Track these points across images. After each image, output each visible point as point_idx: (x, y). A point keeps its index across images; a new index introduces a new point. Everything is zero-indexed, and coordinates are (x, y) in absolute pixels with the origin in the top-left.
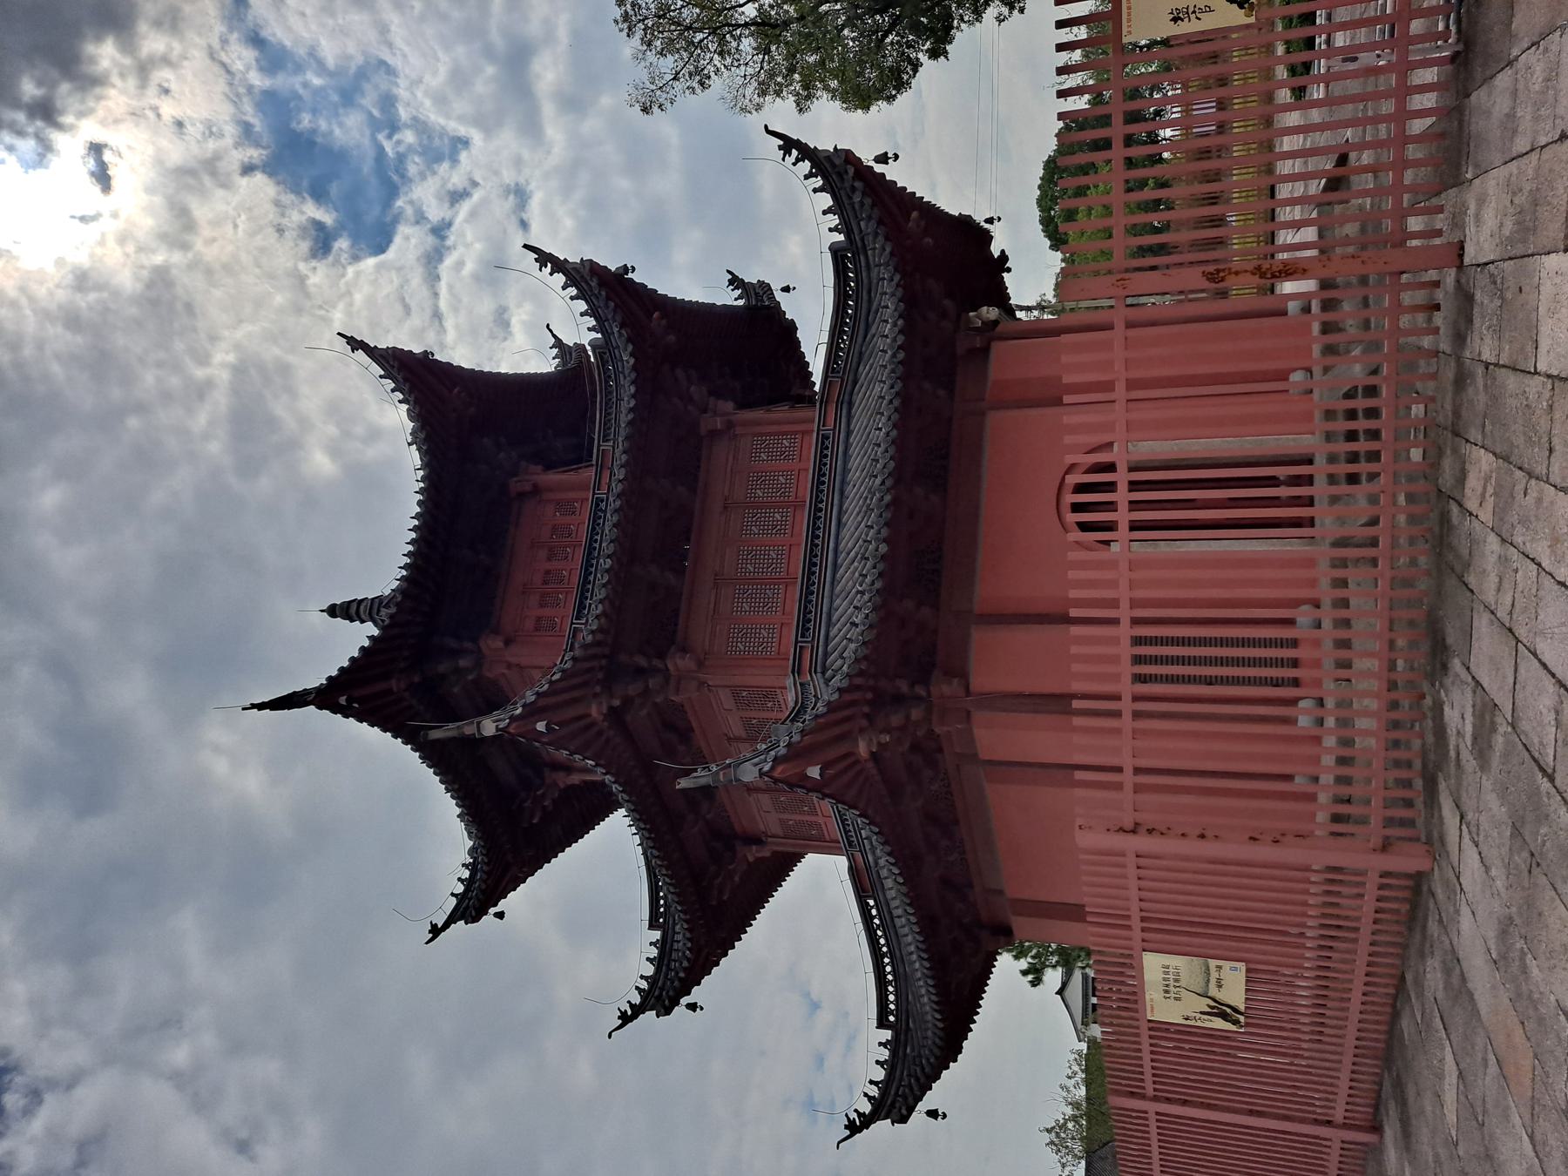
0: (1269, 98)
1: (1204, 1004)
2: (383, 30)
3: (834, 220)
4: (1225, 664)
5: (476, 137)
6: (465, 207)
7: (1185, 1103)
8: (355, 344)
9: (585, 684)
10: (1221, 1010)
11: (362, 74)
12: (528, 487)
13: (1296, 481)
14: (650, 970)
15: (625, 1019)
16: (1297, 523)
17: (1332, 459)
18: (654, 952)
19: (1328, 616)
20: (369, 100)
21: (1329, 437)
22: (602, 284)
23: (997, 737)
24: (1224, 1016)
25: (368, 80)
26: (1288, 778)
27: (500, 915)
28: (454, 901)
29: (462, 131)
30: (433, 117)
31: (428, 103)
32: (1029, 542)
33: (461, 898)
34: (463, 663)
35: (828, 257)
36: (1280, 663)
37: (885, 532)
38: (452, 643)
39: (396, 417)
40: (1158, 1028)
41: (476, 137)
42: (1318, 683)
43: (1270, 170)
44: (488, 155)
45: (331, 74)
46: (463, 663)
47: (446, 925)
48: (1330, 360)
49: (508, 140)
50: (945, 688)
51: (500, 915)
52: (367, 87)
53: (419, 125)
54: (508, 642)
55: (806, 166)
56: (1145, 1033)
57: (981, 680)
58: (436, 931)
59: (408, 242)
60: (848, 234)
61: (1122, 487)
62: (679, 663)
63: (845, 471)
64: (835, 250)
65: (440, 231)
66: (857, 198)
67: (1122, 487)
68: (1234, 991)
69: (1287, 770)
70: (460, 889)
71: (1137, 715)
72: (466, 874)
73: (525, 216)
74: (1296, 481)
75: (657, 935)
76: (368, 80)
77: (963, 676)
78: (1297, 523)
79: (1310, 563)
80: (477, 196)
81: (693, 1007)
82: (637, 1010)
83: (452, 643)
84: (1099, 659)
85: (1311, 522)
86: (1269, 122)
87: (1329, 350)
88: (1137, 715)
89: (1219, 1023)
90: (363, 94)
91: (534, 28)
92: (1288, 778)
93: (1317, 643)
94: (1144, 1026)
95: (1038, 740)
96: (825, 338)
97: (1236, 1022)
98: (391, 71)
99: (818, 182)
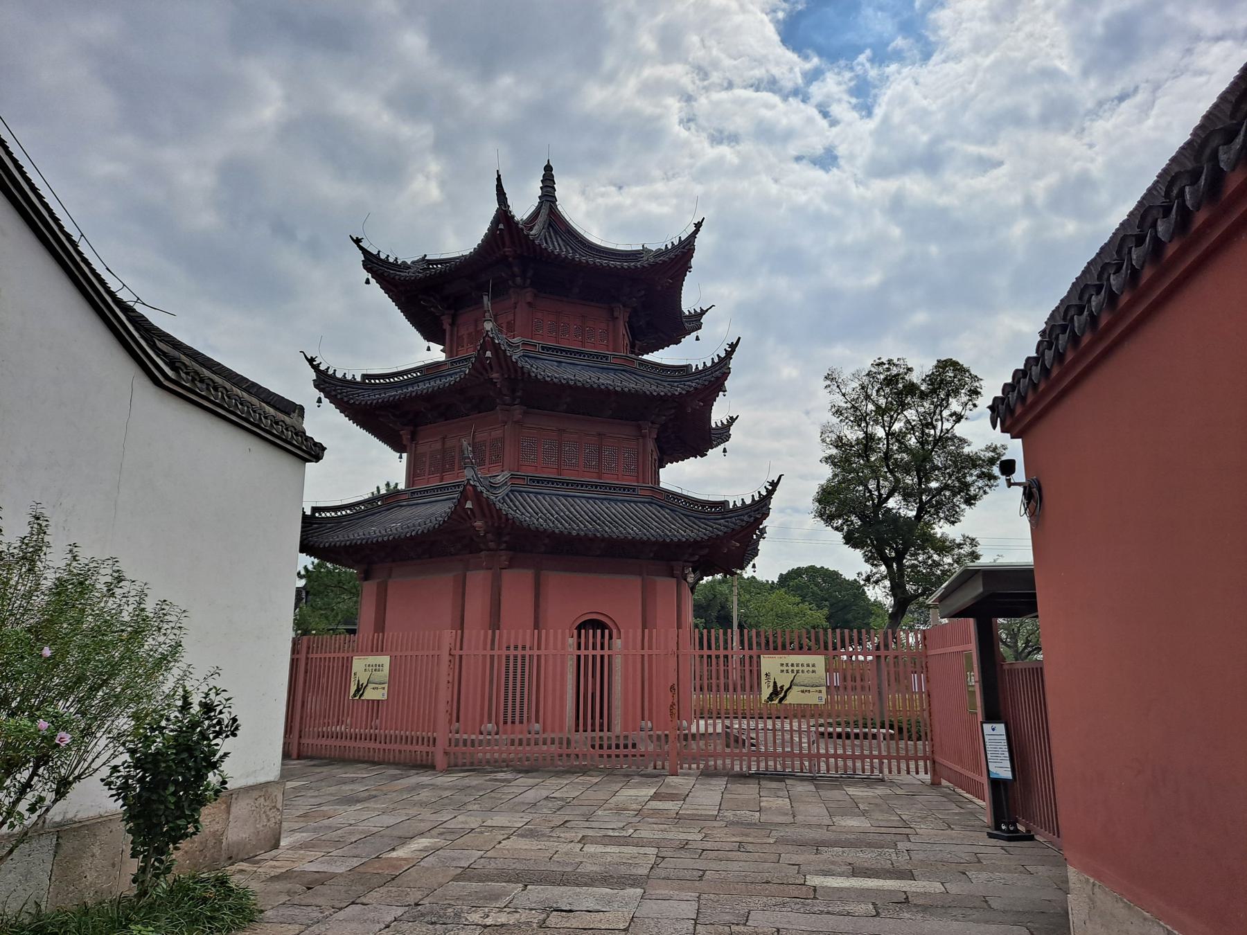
0: (812, 716)
1: (364, 681)
2: (957, 57)
3: (739, 504)
4: (515, 695)
5: (872, 124)
6: (814, 113)
7: (306, 672)
8: (698, 226)
9: (509, 369)
10: (360, 689)
11: (920, 38)
12: (616, 314)
13: (601, 725)
14: (339, 375)
15: (311, 361)
16: (577, 725)
17: (609, 738)
18: (349, 377)
19: (541, 736)
20: (900, 42)
21: (618, 737)
22: (717, 378)
23: (478, 581)
24: (358, 690)
25: (917, 41)
26: (458, 721)
27: (368, 282)
28: (375, 253)
29: (879, 112)
30: (889, 92)
31: (899, 88)
32: (573, 594)
33: (377, 256)
34: (518, 280)
35: (722, 499)
36: (521, 716)
37: (582, 533)
38: (530, 274)
39: (659, 240)
40: (349, 661)
41: (872, 124)
42: (505, 733)
43: (795, 716)
44: (856, 134)
45: (923, 15)
46: (518, 280)
47: (361, 248)
48: (655, 738)
49: (865, 151)
50: (504, 557)
51: (368, 282)
52: (911, 41)
53: (884, 79)
54: (529, 304)
55: (764, 493)
56: (345, 655)
57: (508, 576)
58: (357, 241)
59: (789, 65)
60: (731, 511)
61: (602, 652)
62: (517, 411)
63: (616, 501)
64: (725, 503)
65: (800, 93)
66: (746, 518)
67: (602, 652)
68: (370, 694)
69: (541, 720)
70: (383, 256)
71: (508, 657)
72: (391, 260)
73: (804, 161)
74: (601, 725)
75: (359, 379)
76: (917, 41)
77: (510, 566)
78: (577, 725)
79: (561, 729)
80: (824, 123)
81: (319, 401)
82: (316, 368)
83: (530, 274)
84: (517, 630)
85: (577, 731)
86: (804, 716)
87: (659, 737)
88: (508, 657)
89: (353, 688)
90: (905, 38)
91: (949, 176)
92: (458, 721)
93: (521, 732)
94: (350, 655)
95: (477, 605)
96: (685, 493)
97: (355, 695)
98: (927, 57)
99: (757, 498)
